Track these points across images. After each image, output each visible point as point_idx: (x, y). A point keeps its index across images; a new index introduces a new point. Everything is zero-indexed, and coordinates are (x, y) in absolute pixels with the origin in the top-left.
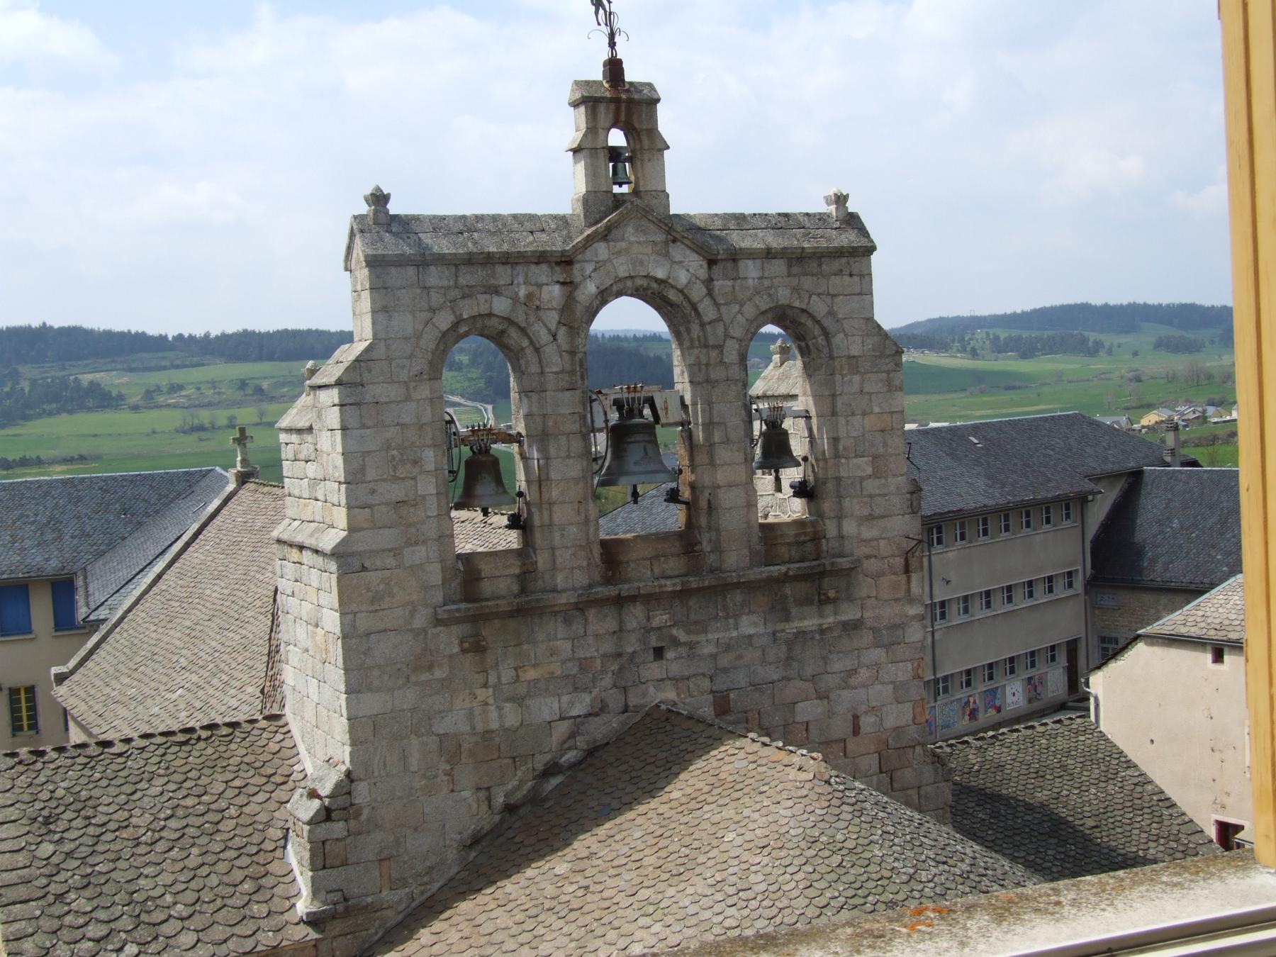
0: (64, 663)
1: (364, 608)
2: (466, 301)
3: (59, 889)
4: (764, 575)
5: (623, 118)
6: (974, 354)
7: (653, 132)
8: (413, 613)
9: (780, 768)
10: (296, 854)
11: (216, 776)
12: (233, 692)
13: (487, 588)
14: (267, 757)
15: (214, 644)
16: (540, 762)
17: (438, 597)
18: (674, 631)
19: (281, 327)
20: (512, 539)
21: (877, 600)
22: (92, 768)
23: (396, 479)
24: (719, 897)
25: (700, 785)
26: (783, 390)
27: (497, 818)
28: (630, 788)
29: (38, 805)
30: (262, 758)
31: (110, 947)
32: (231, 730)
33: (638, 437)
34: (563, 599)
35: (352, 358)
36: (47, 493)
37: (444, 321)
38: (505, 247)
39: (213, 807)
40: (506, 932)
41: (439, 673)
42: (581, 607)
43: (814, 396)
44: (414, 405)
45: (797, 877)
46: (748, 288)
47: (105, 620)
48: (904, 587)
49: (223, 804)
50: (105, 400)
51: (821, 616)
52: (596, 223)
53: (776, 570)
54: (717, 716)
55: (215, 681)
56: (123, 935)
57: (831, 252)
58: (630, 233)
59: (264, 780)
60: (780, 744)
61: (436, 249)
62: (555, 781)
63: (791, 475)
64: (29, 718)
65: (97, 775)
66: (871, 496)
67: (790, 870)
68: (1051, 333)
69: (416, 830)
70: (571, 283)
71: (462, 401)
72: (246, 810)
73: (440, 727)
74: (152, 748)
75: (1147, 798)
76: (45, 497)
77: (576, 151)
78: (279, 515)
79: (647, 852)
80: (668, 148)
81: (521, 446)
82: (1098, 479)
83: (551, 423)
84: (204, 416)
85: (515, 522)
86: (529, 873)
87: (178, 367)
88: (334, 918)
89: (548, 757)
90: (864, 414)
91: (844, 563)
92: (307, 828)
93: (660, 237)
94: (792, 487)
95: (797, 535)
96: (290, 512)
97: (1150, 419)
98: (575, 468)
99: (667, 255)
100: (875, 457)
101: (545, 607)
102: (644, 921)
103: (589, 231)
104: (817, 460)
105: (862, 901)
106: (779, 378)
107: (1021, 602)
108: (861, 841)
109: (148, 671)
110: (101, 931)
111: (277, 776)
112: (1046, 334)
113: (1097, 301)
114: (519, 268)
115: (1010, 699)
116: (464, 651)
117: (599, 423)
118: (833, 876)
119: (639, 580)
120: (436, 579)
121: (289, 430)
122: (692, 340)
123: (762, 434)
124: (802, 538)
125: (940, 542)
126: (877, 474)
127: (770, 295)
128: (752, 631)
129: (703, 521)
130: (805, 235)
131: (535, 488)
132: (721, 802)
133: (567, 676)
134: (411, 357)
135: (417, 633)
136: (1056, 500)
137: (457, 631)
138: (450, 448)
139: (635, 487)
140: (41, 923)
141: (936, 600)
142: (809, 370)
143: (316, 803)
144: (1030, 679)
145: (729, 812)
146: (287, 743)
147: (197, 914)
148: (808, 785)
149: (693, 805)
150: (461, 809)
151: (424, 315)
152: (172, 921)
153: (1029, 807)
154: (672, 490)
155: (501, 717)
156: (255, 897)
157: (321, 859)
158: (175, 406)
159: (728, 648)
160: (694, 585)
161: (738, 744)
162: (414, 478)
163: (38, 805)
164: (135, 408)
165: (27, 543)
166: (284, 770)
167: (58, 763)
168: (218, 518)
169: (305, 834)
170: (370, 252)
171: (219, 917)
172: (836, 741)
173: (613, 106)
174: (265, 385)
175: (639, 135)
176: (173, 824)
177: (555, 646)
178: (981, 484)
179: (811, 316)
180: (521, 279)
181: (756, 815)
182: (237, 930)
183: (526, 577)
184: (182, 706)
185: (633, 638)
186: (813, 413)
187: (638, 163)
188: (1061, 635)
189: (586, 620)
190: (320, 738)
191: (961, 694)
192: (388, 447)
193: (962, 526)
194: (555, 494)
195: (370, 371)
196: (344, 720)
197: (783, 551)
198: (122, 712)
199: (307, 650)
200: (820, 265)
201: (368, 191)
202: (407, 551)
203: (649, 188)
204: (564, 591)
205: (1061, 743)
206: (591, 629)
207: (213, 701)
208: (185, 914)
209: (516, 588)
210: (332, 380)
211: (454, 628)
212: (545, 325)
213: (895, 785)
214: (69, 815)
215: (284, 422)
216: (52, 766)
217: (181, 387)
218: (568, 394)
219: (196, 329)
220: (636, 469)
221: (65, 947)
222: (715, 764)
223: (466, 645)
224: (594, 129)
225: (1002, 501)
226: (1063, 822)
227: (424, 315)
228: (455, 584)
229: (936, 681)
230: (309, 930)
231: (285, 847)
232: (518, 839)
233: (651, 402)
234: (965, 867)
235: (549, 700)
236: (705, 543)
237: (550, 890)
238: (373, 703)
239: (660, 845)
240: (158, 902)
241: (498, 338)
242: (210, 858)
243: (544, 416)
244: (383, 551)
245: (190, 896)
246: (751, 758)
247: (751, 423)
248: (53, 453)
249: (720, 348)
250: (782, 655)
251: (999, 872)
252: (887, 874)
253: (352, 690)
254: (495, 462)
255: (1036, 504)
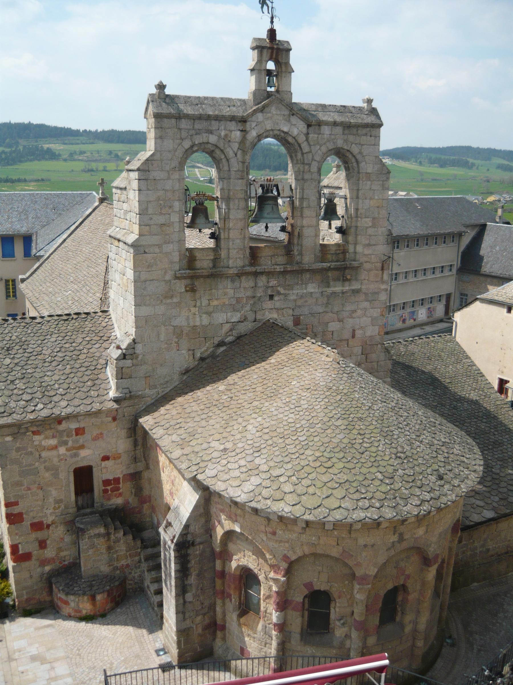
0: (24, 274)
1: (144, 269)
2: (197, 136)
3: (13, 378)
4: (320, 267)
5: (274, 56)
6: (421, 163)
7: (287, 64)
8: (165, 273)
9: (319, 354)
10: (111, 371)
11: (79, 335)
12: (91, 295)
13: (198, 264)
14: (101, 328)
15: (85, 273)
16: (216, 341)
17: (177, 268)
18: (279, 289)
19: (128, 129)
20: (211, 243)
21: (367, 281)
22: (27, 328)
23: (161, 214)
24: (287, 408)
25: (284, 358)
26: (336, 184)
27: (196, 363)
28: (254, 356)
29: (5, 342)
30: (99, 329)
31: (32, 404)
32: (86, 316)
33: (270, 202)
34: (231, 271)
35: (145, 158)
36: (23, 199)
37: (187, 144)
38: (217, 113)
39: (77, 348)
40: (196, 413)
41: (175, 300)
42: (239, 275)
43: (349, 189)
44: (171, 181)
45: (321, 404)
46: (324, 139)
47: (43, 256)
48: (380, 276)
49: (81, 348)
50: (52, 156)
51: (343, 286)
52: (258, 104)
53: (325, 265)
54: (294, 325)
55: (84, 289)
56: (37, 400)
57: (364, 123)
58: (273, 109)
59: (99, 338)
60: (320, 344)
61: (185, 112)
62: (222, 349)
63: (336, 223)
64: (13, 292)
65: (29, 331)
66: (370, 236)
67: (318, 400)
68: (454, 157)
69: (161, 365)
70: (245, 131)
71: (202, 166)
72: (91, 351)
73: (176, 323)
74: (53, 321)
75: (473, 372)
76: (22, 200)
77: (252, 70)
78: (110, 224)
79: (258, 385)
80: (293, 72)
81: (218, 202)
82: (467, 226)
83: (231, 193)
84: (94, 165)
85: (213, 236)
86: (208, 388)
87: (84, 144)
88: (125, 399)
89: (220, 339)
90: (371, 199)
91: (355, 264)
92: (115, 361)
93: (287, 112)
94: (336, 228)
95: (336, 250)
96: (115, 224)
97: (491, 199)
98: (241, 214)
99: (289, 121)
100: (374, 218)
101: (223, 274)
102: (254, 416)
103: (254, 108)
104: (348, 218)
105: (348, 416)
106: (334, 178)
107: (429, 276)
108: (350, 390)
109: (57, 281)
110: (28, 397)
111: (105, 337)
112: (452, 157)
113: (475, 145)
114: (222, 122)
115: (420, 316)
116: (187, 291)
117: (253, 194)
118: (337, 405)
119: (265, 265)
120: (176, 259)
121: (117, 188)
122: (297, 160)
123: (325, 204)
124: (338, 252)
125: (398, 247)
126: (374, 226)
127: (334, 143)
128: (312, 291)
129: (295, 241)
130: (352, 116)
131: (222, 221)
132: (292, 367)
133: (231, 305)
134: (171, 159)
135: (166, 282)
136: (449, 234)
137: (184, 282)
138: (186, 202)
139: (267, 224)
140: (5, 392)
141: (394, 272)
142: (348, 177)
143: (120, 351)
144: (429, 308)
145: (295, 372)
146: (109, 323)
147: (68, 394)
148: (330, 364)
149: (280, 366)
150: (182, 358)
151: (178, 141)
152: (58, 395)
153: (423, 372)
154: (283, 226)
155: (201, 320)
156: (92, 388)
157: (120, 375)
158: (82, 160)
159: (302, 297)
160: (289, 269)
161: (301, 342)
162: (169, 214)
163: (5, 342)
164: (65, 160)
165: (14, 220)
166: (107, 335)
167: (14, 325)
168: (91, 217)
169: (114, 364)
170: (156, 111)
171: (77, 395)
172: (344, 340)
173: (270, 51)
174: (119, 154)
175: (281, 65)
176: (60, 354)
177: (226, 291)
178: (418, 224)
179: (351, 153)
180: (223, 128)
181: (306, 375)
182: (84, 401)
183: (216, 261)
184: (70, 299)
185: (261, 290)
186: (348, 196)
187: (280, 78)
188: (444, 291)
189: (241, 281)
190: (123, 326)
191: (400, 312)
192: (158, 199)
193: (408, 242)
194: (231, 225)
195: (152, 165)
196: (133, 317)
197: (329, 256)
198: (46, 298)
199: (119, 285)
200: (357, 131)
201: (157, 83)
202: (164, 246)
203: (284, 90)
204: (232, 268)
205: (440, 346)
206: (243, 285)
207: (83, 298)
208: (63, 393)
209: (211, 265)
210: (136, 168)
211: (183, 281)
212: (232, 149)
213: (368, 360)
214: (17, 347)
215: (115, 184)
216: (11, 326)
217: (85, 152)
218: (240, 181)
219: (92, 128)
220: (268, 216)
221: (14, 403)
222: (291, 349)
223: (188, 289)
224: (260, 61)
225: (426, 233)
226: (437, 379)
227: (178, 141)
228: (185, 262)
229: (390, 306)
230: (114, 404)
231: (106, 368)
232: (205, 372)
233: (277, 186)
234: (393, 404)
235: (222, 314)
236: (295, 251)
237: (216, 397)
238: (146, 311)
239: (264, 383)
240: (52, 387)
241: (211, 153)
242: (74, 370)
243: (229, 190)
244: (154, 245)
245: (66, 386)
246: (307, 348)
247: (320, 199)
248: (31, 177)
249: (309, 165)
250: (325, 302)
251: (408, 407)
252: (360, 405)
253: (137, 305)
254: (206, 209)
255: (440, 235)
